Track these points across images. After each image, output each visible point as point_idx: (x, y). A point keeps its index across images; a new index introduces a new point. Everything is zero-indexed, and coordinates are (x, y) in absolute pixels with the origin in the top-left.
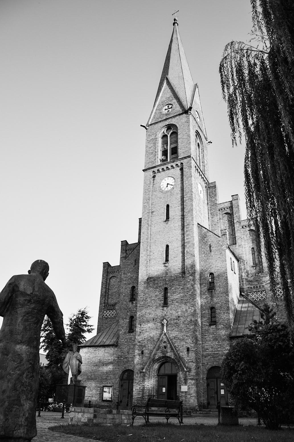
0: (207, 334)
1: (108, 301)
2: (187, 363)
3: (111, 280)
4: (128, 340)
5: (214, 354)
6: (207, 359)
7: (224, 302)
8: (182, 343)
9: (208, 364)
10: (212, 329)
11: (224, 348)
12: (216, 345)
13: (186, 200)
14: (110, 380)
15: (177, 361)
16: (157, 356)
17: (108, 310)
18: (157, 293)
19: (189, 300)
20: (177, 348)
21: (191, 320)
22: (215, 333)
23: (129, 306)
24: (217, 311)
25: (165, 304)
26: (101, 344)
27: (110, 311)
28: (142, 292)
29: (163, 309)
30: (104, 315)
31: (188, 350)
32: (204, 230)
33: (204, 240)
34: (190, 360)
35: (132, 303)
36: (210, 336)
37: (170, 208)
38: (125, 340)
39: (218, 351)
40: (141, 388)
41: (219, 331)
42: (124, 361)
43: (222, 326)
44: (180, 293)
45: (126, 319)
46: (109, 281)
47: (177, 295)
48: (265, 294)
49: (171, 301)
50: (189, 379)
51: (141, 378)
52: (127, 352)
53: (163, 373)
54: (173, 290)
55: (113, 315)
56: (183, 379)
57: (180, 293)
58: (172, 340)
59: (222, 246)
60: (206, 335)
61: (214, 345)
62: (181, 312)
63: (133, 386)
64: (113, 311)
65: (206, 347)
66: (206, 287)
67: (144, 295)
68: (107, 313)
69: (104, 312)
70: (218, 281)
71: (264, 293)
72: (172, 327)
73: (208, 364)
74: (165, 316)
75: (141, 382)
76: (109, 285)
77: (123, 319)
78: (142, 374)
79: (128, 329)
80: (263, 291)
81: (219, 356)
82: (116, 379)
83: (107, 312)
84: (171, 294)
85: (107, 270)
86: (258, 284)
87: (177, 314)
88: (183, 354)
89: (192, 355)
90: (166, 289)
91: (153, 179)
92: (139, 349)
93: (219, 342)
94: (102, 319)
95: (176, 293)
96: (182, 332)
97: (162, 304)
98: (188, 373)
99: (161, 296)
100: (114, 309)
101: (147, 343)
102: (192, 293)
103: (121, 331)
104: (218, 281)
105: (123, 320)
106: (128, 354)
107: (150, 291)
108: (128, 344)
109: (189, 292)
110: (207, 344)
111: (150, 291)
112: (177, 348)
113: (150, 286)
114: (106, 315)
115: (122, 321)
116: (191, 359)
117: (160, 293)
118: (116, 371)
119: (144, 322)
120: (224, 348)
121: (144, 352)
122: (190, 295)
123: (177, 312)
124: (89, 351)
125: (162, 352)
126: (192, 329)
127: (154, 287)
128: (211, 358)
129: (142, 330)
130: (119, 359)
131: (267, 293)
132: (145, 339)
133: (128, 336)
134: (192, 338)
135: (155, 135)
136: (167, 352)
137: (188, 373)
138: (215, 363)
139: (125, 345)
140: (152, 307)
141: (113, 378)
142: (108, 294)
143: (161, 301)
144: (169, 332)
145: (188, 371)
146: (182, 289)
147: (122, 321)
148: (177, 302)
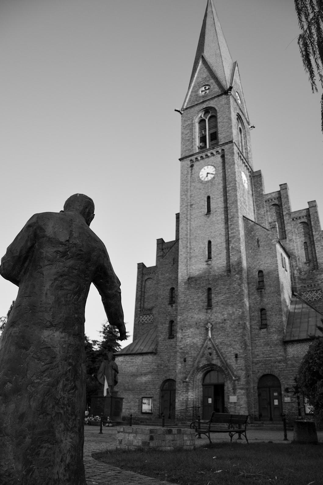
1: (143, 305)
2: (235, 371)
3: (147, 282)
4: (169, 347)
5: (265, 360)
6: (258, 366)
8: (230, 349)
9: (259, 372)
10: (263, 333)
11: (277, 353)
12: (268, 350)
13: (229, 190)
14: (149, 391)
16: (201, 363)
17: (145, 315)
18: (200, 294)
20: (224, 354)
21: (239, 323)
22: (266, 338)
24: (267, 312)
27: (146, 316)
28: (183, 294)
30: (140, 321)
31: (236, 356)
32: (250, 223)
33: (251, 234)
37: (211, 199)
38: (164, 346)
42: (164, 370)
43: (274, 329)
44: (226, 293)
45: (165, 324)
48: (321, 293)
49: (216, 303)
52: (168, 360)
54: (218, 290)
55: (150, 320)
56: (231, 388)
57: (226, 293)
59: (271, 240)
60: (256, 340)
62: (227, 314)
64: (150, 316)
65: (256, 353)
67: (185, 297)
68: (143, 319)
70: (269, 280)
72: (218, 331)
73: (259, 372)
75: (185, 393)
77: (162, 324)
81: (271, 363)
82: (156, 389)
83: (143, 317)
86: (313, 282)
87: (223, 317)
88: (231, 361)
91: (190, 168)
93: (271, 347)
96: (229, 337)
99: (204, 297)
101: (190, 349)
103: (161, 337)
104: (269, 280)
105: (162, 325)
106: (169, 362)
109: (236, 292)
112: (224, 354)
114: (143, 321)
115: (161, 326)
116: (240, 367)
117: (203, 295)
119: (185, 326)
120: (277, 353)
124: (125, 360)
127: (195, 288)
130: (159, 368)
134: (241, 343)
135: (191, 120)
136: (213, 359)
137: (236, 382)
138: (267, 371)
139: (165, 352)
143: (204, 302)
144: (214, 337)
145: (237, 380)
146: (228, 289)
147: (161, 326)
148: (222, 304)
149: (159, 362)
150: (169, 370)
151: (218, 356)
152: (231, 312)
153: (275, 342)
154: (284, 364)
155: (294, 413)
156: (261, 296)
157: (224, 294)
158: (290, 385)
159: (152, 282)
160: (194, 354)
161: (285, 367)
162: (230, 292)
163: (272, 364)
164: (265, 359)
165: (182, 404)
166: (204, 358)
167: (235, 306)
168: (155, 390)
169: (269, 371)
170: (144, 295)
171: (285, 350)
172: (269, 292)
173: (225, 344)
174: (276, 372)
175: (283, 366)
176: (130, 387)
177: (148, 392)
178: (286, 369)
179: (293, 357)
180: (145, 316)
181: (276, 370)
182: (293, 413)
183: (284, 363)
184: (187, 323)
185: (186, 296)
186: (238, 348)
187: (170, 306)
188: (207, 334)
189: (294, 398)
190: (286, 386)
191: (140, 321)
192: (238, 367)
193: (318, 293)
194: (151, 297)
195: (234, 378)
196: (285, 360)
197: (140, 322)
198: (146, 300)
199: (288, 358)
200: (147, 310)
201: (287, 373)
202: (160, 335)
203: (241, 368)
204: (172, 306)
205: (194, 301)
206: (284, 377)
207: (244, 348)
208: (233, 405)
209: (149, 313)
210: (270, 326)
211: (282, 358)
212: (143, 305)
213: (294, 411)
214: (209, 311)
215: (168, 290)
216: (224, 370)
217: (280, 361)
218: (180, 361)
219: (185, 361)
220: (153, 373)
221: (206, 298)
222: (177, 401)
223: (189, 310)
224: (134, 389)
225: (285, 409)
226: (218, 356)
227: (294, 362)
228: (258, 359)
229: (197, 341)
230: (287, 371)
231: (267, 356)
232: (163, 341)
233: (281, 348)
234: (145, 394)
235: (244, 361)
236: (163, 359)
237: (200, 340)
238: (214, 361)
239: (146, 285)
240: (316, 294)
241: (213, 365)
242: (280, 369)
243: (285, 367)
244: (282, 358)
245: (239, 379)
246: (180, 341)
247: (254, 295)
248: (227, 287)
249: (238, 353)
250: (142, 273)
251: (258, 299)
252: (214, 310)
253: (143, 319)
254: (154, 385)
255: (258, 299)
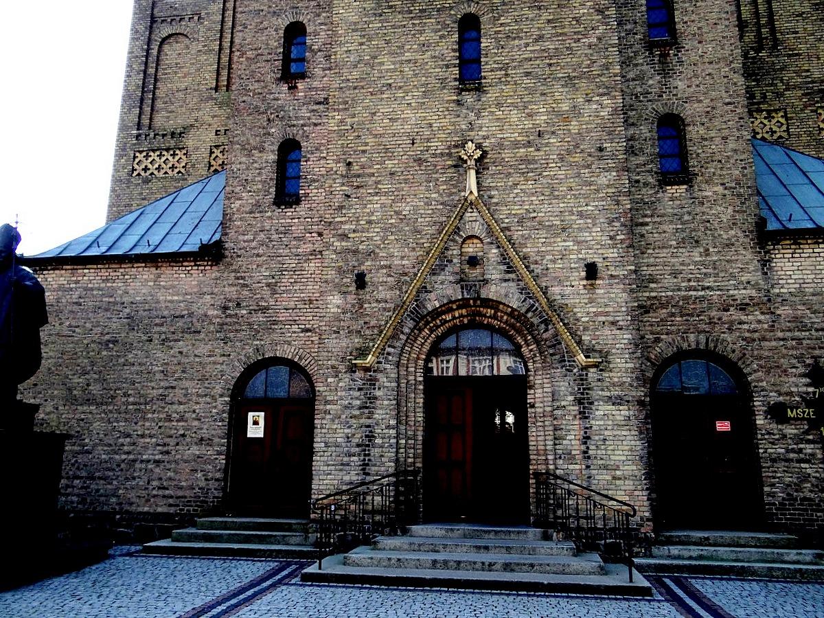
0: (649, 220)
1: (151, 119)
2: (586, 329)
3: (166, 48)
4: (275, 237)
5: (686, 298)
7: (724, 95)
8: (560, 244)
9: (657, 340)
10: (672, 199)
11: (733, 276)
12: (696, 263)
14: (180, 403)
15: (536, 321)
16: (432, 296)
17: (154, 151)
18: (429, 36)
19: (589, 66)
20: (536, 263)
21: (601, 149)
22: (686, 217)
23: (277, 99)
24: (690, 128)
25: (469, 73)
26: (137, 251)
27: (160, 156)
28: (353, 31)
29: (458, 103)
30: (134, 170)
31: (592, 271)
34: (603, 319)
35: (290, 88)
36: (665, 227)
38: (256, 234)
39: (703, 289)
40: (355, 441)
41: (704, 209)
42: (250, 324)
43: (720, 189)
44: (541, 37)
45: (262, 150)
46: (159, 52)
47: (527, 45)
48: (783, 121)
49: (501, 69)
50: (601, 399)
51: (357, 394)
52: (268, 285)
53: (261, 393)
54: (508, 24)
55: (173, 167)
56: (571, 398)
57: (541, 37)
58: (508, 229)
60: (647, 224)
61: (682, 264)
62: (548, 113)
63: (313, 427)
64: (174, 155)
66: (638, 37)
67: (362, 44)
68: (147, 163)
69: (135, 157)
70: (694, 17)
71: (779, 117)
74: (471, 130)
75: (357, 412)
76: (158, 65)
77: (247, 150)
78: (359, 374)
79: (273, 190)
80: (776, 111)
81: (710, 308)
82: (213, 397)
83: (147, 156)
84: (497, 40)
85: (153, 9)
86: (758, 86)
87: (528, 124)
88: (568, 290)
89: (614, 297)
90: (469, 27)
92: (340, 268)
93: (707, 252)
94: (129, 181)
95: (521, 38)
96: (557, 197)
97: (455, 79)
98: (593, 374)
99: (448, 47)
100: (180, 149)
101: (383, 239)
102: (599, 39)
103: (240, 199)
104: (694, 17)
105: (249, 155)
106: (274, 292)
107: (393, 27)
108: (271, 252)
109: (585, 36)
110: (652, 260)
111: (393, 27)
112: (536, 263)
113: (391, 7)
114: (146, 169)
115: (244, 159)
116: (607, 314)
117: (442, 37)
118: (215, 363)
119: (364, 152)
120: (733, 276)
121: (367, 279)
122: (590, 46)
123: (530, 115)
124: (77, 282)
125: (457, 282)
126: (608, 186)
127: (411, 12)
128: (673, 315)
129: (358, 187)
130: (230, 316)
131: (792, 118)
132: (369, 222)
133: (270, 218)
134: (610, 222)
136: (486, 282)
137: (593, 374)
138: (692, 337)
139: (258, 255)
140: (406, 92)
141: (198, 396)
142: (154, 94)
143: (447, 66)
144: (491, 197)
145: (596, 366)
146: (549, 21)
147: (244, 159)
148: (528, 74)
149: (232, 292)
150: (275, 323)
151: (510, 269)
152: (565, 107)
153: (725, 237)
154: (762, 317)
155: (810, 499)
156: (665, 71)
157: (536, 41)
158: (790, 394)
159: (187, 47)
160: (402, 258)
161: (766, 326)
162: (561, 34)
163: (713, 313)
164: (683, 293)
165: (346, 459)
166: (447, 276)
167: (583, 84)
168: (208, 399)
169: (702, 338)
170: (155, 88)
171: (765, 264)
172: (694, 58)
173: (540, 223)
174: (731, 343)
175: (759, 322)
176: (95, 389)
177: (175, 407)
178: (769, 335)
179: (801, 291)
180: (154, 155)
181: (727, 337)
182: (805, 499)
183: (762, 313)
184: (371, 140)
185: (370, 40)
186: (598, 241)
187: (285, 87)
188: (460, 185)
189: (809, 442)
190: (774, 398)
191: (134, 170)
192: (596, 314)
193: (774, 121)
194: (181, 95)
195: (581, 357)
196: (767, 302)
197: (135, 173)
198: (159, 104)
199: (778, 295)
200: (164, 136)
201: (777, 348)
202: (237, 189)
203: (610, 319)
204: (293, 88)
205: (404, 58)
206: (762, 362)
207: (622, 241)
208: (578, 467)
209: (172, 143)
210: (700, 178)
211: (754, 293)
212: (151, 119)
213: (811, 491)
214: (469, 98)
215: (276, 30)
216: (532, 326)
217: (747, 304)
218: (336, 286)
219: (361, 282)
220: (202, 336)
221: (454, 50)
222: (318, 445)
223: (382, 93)
224: (113, 397)
225: (773, 485)
226: (510, 269)
227: (801, 310)
228: (653, 294)
229: (416, 208)
230: (774, 343)
231: (692, 284)
232: (251, 213)
233: (749, 256)
234: (163, 416)
235: (624, 291)
236: (249, 282)
237: (427, 204)
238: (493, 288)
239: (163, 57)
240: (766, 122)
241: (488, 303)
242: (747, 335)
243: (766, 326)
244: (754, 293)
245: (603, 365)
246: (341, 208)
247: (636, 65)
248: (546, 16)
249: (598, 260)
250: (152, 14)
251: (651, 82)
252: (491, 95)
253: (147, 163)
254: (202, 379)
255: (651, 82)
